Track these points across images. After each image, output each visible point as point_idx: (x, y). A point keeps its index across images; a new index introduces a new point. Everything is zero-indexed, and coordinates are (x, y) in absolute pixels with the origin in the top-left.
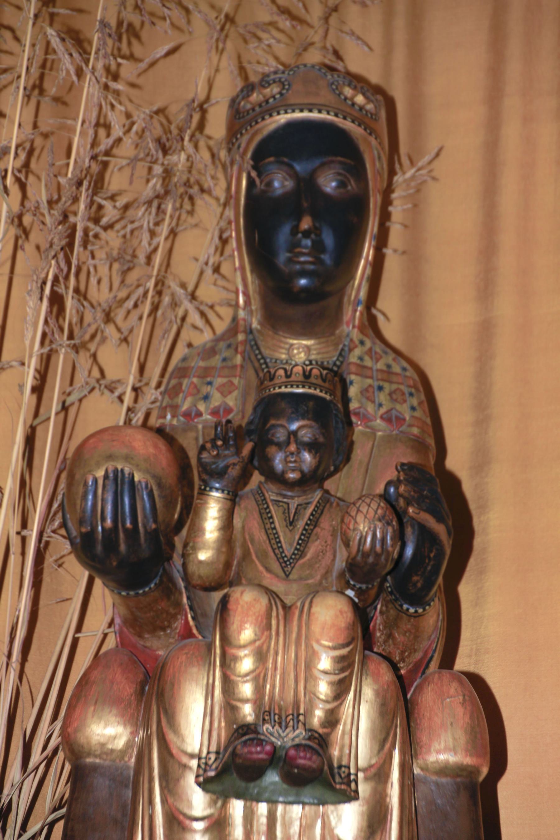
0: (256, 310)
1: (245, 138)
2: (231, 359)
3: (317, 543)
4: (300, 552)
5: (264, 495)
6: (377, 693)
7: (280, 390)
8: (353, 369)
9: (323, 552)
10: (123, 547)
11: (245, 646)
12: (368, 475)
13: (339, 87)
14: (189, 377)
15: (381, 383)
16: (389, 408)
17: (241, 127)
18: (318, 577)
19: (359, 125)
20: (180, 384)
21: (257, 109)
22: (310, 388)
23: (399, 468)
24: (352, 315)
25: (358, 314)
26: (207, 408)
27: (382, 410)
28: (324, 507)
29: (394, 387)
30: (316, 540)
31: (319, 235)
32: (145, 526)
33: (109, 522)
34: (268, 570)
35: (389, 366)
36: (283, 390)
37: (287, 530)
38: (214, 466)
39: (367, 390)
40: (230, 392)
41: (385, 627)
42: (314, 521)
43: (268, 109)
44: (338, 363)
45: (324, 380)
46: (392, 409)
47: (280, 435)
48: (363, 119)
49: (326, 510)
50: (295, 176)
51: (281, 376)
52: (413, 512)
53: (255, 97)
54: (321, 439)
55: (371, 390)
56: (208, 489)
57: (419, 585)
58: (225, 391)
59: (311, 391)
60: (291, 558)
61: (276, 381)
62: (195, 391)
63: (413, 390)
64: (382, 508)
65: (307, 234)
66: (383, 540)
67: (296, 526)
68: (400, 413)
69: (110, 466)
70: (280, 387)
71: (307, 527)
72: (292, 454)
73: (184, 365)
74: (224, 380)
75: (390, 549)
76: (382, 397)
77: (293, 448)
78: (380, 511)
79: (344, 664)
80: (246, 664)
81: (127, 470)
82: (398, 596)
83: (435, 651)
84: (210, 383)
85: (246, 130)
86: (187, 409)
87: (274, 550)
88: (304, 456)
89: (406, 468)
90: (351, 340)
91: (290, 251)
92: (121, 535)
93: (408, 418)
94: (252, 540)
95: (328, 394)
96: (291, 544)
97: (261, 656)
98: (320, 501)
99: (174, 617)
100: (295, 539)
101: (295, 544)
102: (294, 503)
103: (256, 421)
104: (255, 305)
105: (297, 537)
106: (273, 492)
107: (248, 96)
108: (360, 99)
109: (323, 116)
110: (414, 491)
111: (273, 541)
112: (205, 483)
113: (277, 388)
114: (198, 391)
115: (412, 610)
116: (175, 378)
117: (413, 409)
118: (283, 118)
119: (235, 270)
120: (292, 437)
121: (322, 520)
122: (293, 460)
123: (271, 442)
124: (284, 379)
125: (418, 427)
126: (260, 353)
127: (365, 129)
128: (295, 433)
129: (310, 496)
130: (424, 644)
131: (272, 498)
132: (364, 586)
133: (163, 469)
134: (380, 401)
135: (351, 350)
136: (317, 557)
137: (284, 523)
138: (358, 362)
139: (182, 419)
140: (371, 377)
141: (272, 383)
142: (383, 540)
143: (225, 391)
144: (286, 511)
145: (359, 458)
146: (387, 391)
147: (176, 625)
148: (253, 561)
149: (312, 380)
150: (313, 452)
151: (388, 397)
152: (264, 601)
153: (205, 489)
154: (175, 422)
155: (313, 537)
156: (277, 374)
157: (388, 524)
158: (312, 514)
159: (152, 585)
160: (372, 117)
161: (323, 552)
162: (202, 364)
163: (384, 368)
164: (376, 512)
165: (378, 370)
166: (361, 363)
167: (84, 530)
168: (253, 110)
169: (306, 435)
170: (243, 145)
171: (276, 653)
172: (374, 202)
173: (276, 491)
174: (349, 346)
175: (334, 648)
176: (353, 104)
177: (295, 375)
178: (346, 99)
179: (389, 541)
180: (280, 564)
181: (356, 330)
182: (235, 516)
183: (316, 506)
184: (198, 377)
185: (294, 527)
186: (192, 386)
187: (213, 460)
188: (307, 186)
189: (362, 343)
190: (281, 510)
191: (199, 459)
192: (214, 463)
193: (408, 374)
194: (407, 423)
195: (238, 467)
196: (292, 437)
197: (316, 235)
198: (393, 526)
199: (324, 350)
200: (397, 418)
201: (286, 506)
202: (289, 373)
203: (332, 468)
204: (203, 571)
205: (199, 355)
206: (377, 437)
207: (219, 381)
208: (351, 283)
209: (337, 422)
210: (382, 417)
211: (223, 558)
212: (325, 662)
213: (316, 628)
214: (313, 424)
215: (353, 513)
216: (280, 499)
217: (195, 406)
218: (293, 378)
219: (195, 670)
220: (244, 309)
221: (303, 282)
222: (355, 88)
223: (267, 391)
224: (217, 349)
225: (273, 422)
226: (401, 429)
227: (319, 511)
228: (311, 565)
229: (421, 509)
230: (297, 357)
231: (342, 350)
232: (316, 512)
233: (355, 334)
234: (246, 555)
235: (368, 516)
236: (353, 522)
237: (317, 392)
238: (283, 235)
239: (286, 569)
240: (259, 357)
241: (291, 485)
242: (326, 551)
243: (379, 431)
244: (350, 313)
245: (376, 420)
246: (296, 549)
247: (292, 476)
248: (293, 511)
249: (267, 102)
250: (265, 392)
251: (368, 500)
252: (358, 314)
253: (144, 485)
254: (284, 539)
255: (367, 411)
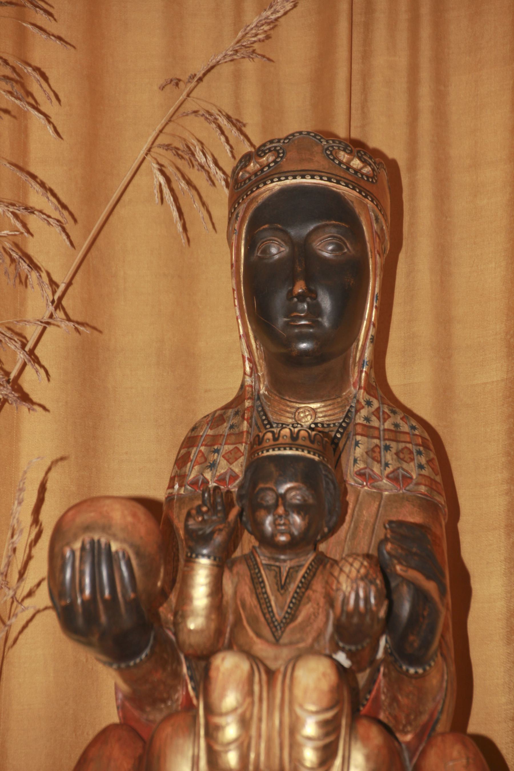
0: (263, 375)
1: (243, 206)
2: (238, 425)
3: (309, 606)
4: (292, 616)
5: (256, 560)
6: (368, 758)
7: (268, 454)
8: (359, 429)
9: (316, 615)
10: (103, 619)
11: (227, 714)
12: (374, 536)
13: (334, 153)
14: (198, 446)
15: (388, 443)
16: (395, 467)
17: (238, 198)
18: (310, 640)
19: (354, 189)
20: (189, 453)
21: (253, 178)
22: (297, 450)
23: (387, 526)
24: (359, 375)
25: (364, 374)
26: (213, 476)
27: (389, 470)
28: (317, 569)
29: (402, 445)
30: (308, 603)
31: (315, 298)
32: (124, 596)
33: (87, 592)
34: (259, 635)
35: (396, 425)
36: (271, 452)
37: (278, 594)
38: (200, 533)
39: (373, 450)
40: (236, 459)
41: (388, 690)
42: (306, 584)
43: (263, 177)
44: (344, 425)
45: (312, 442)
46: (398, 468)
47: (270, 498)
48: (355, 180)
49: (319, 572)
50: (290, 241)
51: (269, 440)
52: (401, 570)
53: (252, 166)
54: (311, 501)
55: (377, 450)
56: (194, 556)
57: (416, 645)
58: (231, 458)
59: (299, 453)
60: (282, 622)
61: (265, 445)
62: (203, 460)
63: (421, 448)
64: (365, 567)
65: (301, 298)
66: (367, 599)
67: (287, 589)
68: (407, 472)
69: (87, 537)
70: (268, 451)
71: (298, 590)
72: (280, 516)
73: (194, 434)
74: (231, 447)
75: (374, 608)
76: (389, 457)
77: (281, 510)
78: (363, 571)
79: (330, 727)
80: (231, 731)
81: (103, 541)
82: (397, 657)
83: (441, 712)
84: (217, 451)
85: (243, 199)
86: (194, 478)
87: (264, 615)
88: (293, 517)
89: (394, 525)
90: (358, 401)
91: (286, 316)
92: (101, 607)
93: (414, 477)
94: (244, 606)
95: (317, 455)
96: (282, 608)
97: (244, 723)
98: (313, 563)
99: (174, 688)
100: (286, 602)
101: (286, 608)
102: (286, 566)
103: (247, 484)
104: (262, 371)
105: (288, 600)
106: (265, 556)
107: (246, 166)
108: (356, 163)
109: (317, 181)
110: (402, 548)
111: (264, 606)
112: (192, 550)
113: (265, 452)
114: (206, 459)
115: (412, 671)
116: (184, 448)
117: (421, 467)
118: (276, 186)
119: (240, 337)
120: (280, 500)
121: (314, 582)
122: (282, 522)
123: (260, 506)
124: (272, 442)
125: (425, 485)
126: (267, 418)
127: (360, 192)
128: (283, 496)
129: (302, 559)
130: (430, 706)
131: (264, 562)
132: (353, 648)
133: (141, 538)
134: (387, 461)
135: (357, 411)
136: (308, 621)
137: (276, 587)
138: (365, 422)
139: (189, 488)
140: (379, 438)
141: (261, 447)
142: (367, 599)
143: (231, 458)
144: (278, 575)
145: (365, 518)
146: (394, 450)
147: (176, 697)
148: (244, 628)
149: (300, 442)
150: (302, 514)
151: (395, 457)
152: (245, 666)
153: (191, 556)
154: (182, 492)
155: (305, 600)
156: (266, 437)
157: (372, 582)
158: (304, 577)
159: (143, 656)
160: (368, 180)
161: (316, 615)
162: (210, 432)
163: (392, 428)
164: (358, 571)
165: (385, 430)
166: (368, 424)
167: (63, 603)
168: (249, 179)
169: (296, 497)
170: (240, 215)
171: (260, 720)
172: (374, 264)
173: (268, 554)
174: (356, 407)
175: (317, 713)
176: (348, 168)
177: (283, 437)
178: (341, 163)
179: (373, 601)
180: (271, 629)
181: (362, 391)
182: (225, 581)
183: (308, 568)
184: (206, 445)
185: (285, 591)
186: (200, 454)
187: (200, 526)
188: (302, 251)
189: (369, 403)
190: (273, 573)
191: (186, 526)
192: (200, 529)
193: (417, 432)
194: (414, 482)
195: (224, 533)
196: (280, 500)
197: (311, 298)
198: (376, 585)
199: (330, 413)
200: (404, 476)
201: (277, 570)
202: (277, 436)
203: (326, 530)
204: (194, 640)
205: (208, 424)
206: (384, 497)
207: (227, 448)
208: (355, 344)
209: (327, 483)
210: (388, 477)
211: (213, 626)
212: (310, 728)
213: (298, 692)
214: (302, 485)
215: (336, 574)
216: (272, 563)
217: (203, 475)
218: (281, 440)
219: (181, 741)
220: (250, 376)
221: (304, 346)
222: (351, 153)
223: (256, 455)
224: (225, 416)
225: (261, 486)
226: (407, 488)
227: (312, 574)
228: (302, 628)
229: (409, 566)
230: (303, 420)
231: (349, 411)
232: (308, 574)
233: (362, 395)
234: (238, 621)
235: (351, 576)
236: (335, 582)
237: (305, 454)
238: (279, 300)
239: (276, 634)
240: (266, 422)
241: (282, 548)
242: (318, 614)
243: (386, 490)
244: (356, 374)
245: (381, 481)
246: (287, 612)
247: (283, 539)
248: (284, 574)
249: (262, 170)
250: (255, 456)
251: (351, 560)
252: (364, 374)
253: (121, 555)
254: (276, 603)
255: (372, 471)
